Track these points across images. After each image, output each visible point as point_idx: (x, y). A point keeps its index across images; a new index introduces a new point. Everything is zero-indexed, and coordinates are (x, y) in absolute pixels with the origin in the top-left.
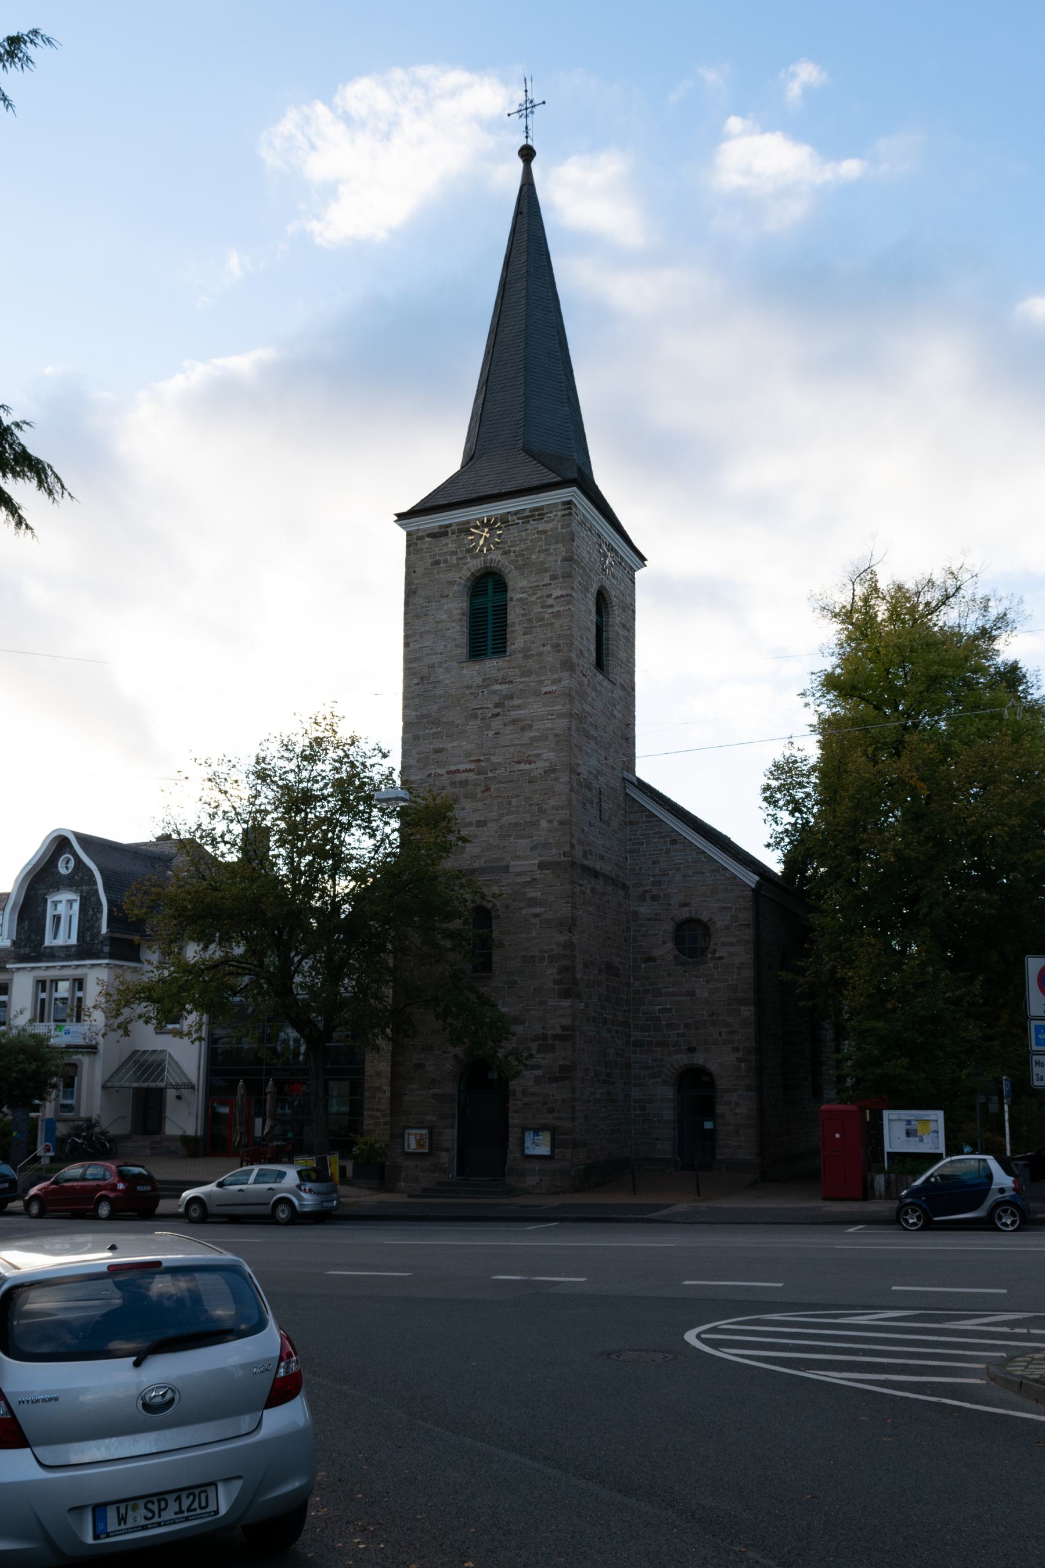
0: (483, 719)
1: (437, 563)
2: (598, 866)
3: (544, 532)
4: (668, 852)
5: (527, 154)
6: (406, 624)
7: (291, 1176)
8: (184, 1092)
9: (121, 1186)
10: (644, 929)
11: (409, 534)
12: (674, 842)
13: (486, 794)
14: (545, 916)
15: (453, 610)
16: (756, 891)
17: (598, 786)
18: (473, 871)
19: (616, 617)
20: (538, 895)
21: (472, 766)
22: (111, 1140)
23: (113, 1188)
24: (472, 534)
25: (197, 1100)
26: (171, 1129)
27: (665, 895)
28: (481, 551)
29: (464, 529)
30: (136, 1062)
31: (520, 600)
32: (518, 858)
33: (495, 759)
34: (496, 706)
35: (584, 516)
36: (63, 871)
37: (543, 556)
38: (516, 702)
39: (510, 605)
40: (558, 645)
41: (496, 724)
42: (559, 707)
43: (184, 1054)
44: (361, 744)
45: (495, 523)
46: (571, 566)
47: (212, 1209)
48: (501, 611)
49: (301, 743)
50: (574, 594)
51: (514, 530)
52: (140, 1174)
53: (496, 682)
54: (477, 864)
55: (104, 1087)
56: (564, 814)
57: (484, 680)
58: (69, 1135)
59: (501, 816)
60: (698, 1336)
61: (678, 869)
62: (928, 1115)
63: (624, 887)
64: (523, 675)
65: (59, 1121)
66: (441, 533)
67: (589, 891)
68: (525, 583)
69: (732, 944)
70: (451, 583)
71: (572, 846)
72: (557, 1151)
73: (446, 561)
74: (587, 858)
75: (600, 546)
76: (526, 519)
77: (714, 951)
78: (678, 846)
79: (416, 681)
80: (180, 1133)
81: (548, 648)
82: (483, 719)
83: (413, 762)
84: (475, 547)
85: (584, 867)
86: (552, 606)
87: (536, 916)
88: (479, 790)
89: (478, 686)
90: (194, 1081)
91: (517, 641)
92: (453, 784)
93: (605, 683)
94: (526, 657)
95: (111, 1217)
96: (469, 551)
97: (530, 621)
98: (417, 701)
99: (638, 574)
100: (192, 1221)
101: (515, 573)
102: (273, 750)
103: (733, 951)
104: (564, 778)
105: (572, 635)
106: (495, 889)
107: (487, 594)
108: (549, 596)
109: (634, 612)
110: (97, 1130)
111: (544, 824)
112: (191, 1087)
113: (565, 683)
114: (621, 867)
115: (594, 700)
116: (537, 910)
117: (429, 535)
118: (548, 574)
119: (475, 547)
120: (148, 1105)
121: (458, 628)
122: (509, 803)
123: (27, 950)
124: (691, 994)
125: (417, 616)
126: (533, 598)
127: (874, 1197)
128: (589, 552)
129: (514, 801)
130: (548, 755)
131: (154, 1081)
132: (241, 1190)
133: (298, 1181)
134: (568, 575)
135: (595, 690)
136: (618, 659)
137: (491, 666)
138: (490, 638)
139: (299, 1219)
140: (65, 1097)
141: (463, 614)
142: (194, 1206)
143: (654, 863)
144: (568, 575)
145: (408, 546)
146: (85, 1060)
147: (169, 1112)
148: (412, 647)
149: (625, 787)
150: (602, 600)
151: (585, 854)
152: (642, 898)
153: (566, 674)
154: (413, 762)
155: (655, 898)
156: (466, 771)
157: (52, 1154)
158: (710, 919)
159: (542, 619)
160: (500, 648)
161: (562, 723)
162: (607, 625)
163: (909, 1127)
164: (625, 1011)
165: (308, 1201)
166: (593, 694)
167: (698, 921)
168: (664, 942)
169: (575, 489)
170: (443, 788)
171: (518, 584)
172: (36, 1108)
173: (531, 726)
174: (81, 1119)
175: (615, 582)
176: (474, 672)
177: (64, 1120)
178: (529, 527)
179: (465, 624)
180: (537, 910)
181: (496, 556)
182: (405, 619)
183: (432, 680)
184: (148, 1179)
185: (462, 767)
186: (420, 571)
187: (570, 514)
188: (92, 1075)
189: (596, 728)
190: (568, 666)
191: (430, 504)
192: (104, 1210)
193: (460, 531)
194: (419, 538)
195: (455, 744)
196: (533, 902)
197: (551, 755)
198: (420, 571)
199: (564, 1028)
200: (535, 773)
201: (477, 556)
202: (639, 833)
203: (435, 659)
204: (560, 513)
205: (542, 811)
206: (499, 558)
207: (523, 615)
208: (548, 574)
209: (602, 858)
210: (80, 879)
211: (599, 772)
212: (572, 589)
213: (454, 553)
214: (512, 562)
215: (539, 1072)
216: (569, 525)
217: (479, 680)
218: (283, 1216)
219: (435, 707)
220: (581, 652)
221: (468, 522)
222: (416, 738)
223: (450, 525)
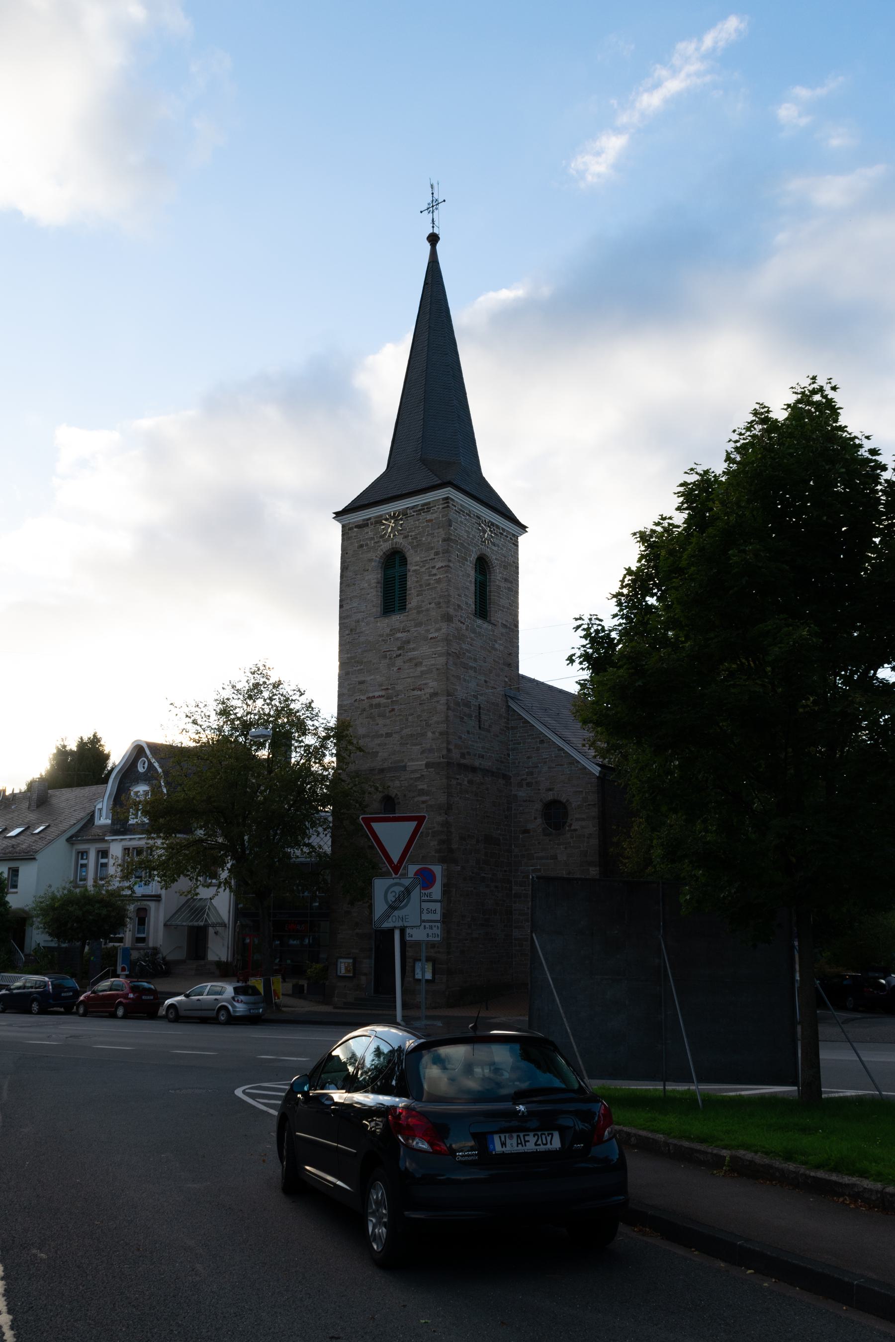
0: (390, 658)
1: (361, 546)
2: (477, 763)
3: (431, 521)
4: (538, 749)
5: (433, 239)
6: (341, 591)
7: (229, 990)
8: (219, 929)
9: (131, 996)
11: (343, 526)
12: (542, 742)
13: (393, 713)
14: (430, 803)
15: (372, 579)
16: (602, 779)
17: (477, 704)
18: (382, 771)
19: (497, 575)
20: (425, 787)
21: (383, 693)
22: (166, 963)
23: (125, 996)
24: (384, 524)
25: (228, 935)
26: (211, 957)
27: (536, 782)
28: (389, 536)
29: (378, 521)
30: (189, 906)
31: (415, 571)
32: (412, 760)
33: (399, 687)
34: (399, 649)
35: (461, 505)
36: (141, 769)
37: (429, 538)
38: (412, 646)
39: (409, 574)
40: (439, 603)
41: (399, 662)
42: (440, 649)
43: (221, 902)
44: (285, 686)
45: (399, 515)
46: (449, 545)
47: (182, 1013)
48: (404, 578)
49: (243, 686)
50: (451, 565)
51: (411, 521)
52: (150, 989)
53: (399, 631)
54: (386, 765)
55: (165, 925)
56: (443, 727)
57: (391, 630)
58: (138, 960)
59: (402, 729)
60: (244, 1092)
61: (545, 762)
63: (505, 777)
64: (415, 626)
65: (132, 949)
66: (362, 526)
67: (466, 783)
68: (418, 558)
69: (583, 819)
70: (370, 560)
71: (449, 750)
72: (436, 976)
73: (367, 545)
74: (465, 758)
75: (480, 525)
76: (419, 512)
77: (571, 825)
78: (545, 745)
79: (347, 632)
80: (217, 959)
81: (433, 605)
82: (390, 658)
83: (346, 691)
84: (385, 534)
85: (460, 765)
86: (435, 575)
87: (423, 802)
88: (388, 710)
89: (388, 635)
90: (226, 921)
91: (413, 601)
92: (371, 706)
93: (486, 625)
94: (419, 613)
95: (125, 1017)
96: (382, 537)
97: (421, 586)
98: (348, 647)
99: (522, 539)
100: (171, 1021)
101: (412, 551)
102: (228, 693)
103: (583, 824)
104: (443, 699)
105: (449, 595)
106: (397, 783)
107: (394, 562)
108: (434, 567)
109: (517, 568)
110: (160, 956)
111: (430, 734)
112: (224, 925)
113: (444, 631)
114: (502, 762)
116: (424, 798)
117: (357, 527)
118: (433, 551)
119: (385, 534)
120: (197, 938)
121: (375, 593)
122: (407, 720)
123: (119, 827)
124: (555, 857)
125: (348, 585)
126: (423, 569)
128: (467, 532)
129: (410, 718)
130: (433, 685)
131: (197, 921)
132: (198, 1000)
133: (233, 995)
134: (446, 551)
135: (474, 631)
136: (499, 605)
137: (396, 619)
138: (397, 599)
139: (234, 1020)
140: (138, 933)
141: (378, 583)
142: (171, 1011)
143: (528, 758)
144: (446, 551)
145: (343, 535)
146: (152, 905)
147: (210, 945)
148: (346, 607)
149: (507, 702)
150: (482, 565)
151: (463, 756)
152: (520, 785)
153: (444, 625)
154: (346, 691)
155: (529, 785)
156: (379, 697)
157: (127, 973)
158: (568, 801)
159: (429, 584)
160: (403, 608)
161: (442, 660)
162: (490, 582)
164: (505, 871)
165: (240, 1008)
166: (473, 635)
167: (559, 802)
168: (535, 818)
171: (414, 559)
172: (121, 940)
173: (421, 663)
174: (149, 948)
175: (495, 548)
176: (385, 625)
177: (138, 949)
179: (379, 589)
180: (424, 798)
181: (399, 539)
182: (341, 588)
183: (358, 631)
184: (149, 991)
185: (377, 694)
186: (350, 552)
187: (448, 506)
188: (158, 916)
189: (475, 660)
190: (448, 618)
191: (357, 504)
192: (120, 1012)
193: (376, 522)
194: (351, 529)
195: (372, 677)
196: (422, 792)
197: (434, 684)
198: (350, 552)
200: (424, 697)
201: (385, 541)
202: (518, 735)
203: (359, 616)
204: (441, 506)
205: (428, 725)
206: (401, 541)
207: (417, 582)
208: (433, 551)
209: (483, 757)
210: (149, 776)
212: (449, 561)
213: (372, 539)
214: (410, 543)
216: (447, 515)
217: (388, 631)
218: (223, 1018)
219: (360, 651)
220: (459, 606)
221: (381, 516)
222: (347, 674)
223: (370, 519)
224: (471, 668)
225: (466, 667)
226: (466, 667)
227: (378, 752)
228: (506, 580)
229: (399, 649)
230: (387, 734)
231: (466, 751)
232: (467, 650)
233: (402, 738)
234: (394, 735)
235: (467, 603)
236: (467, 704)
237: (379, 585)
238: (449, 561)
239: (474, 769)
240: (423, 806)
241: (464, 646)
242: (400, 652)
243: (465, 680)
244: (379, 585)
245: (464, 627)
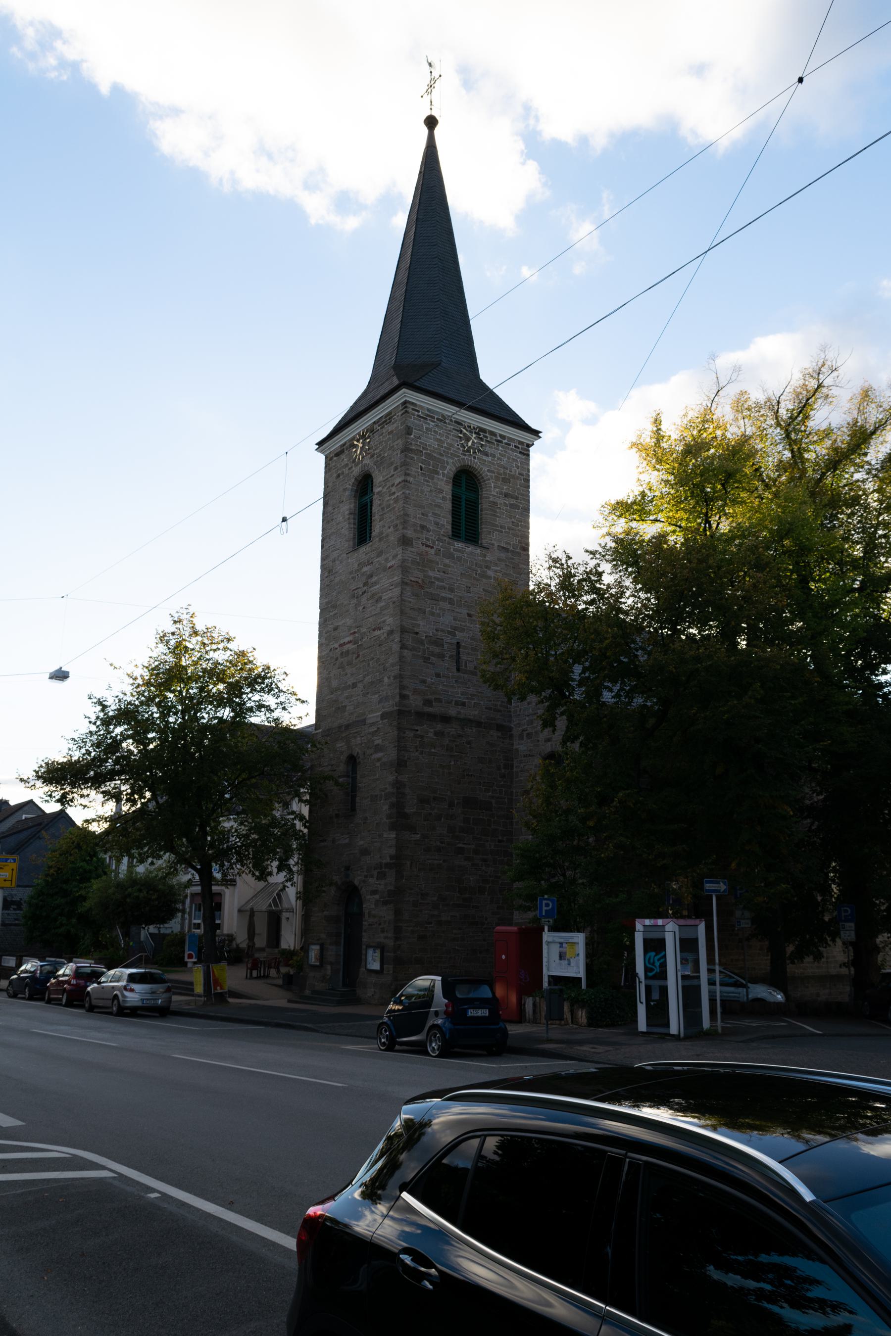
1: (338, 476)
2: (453, 712)
3: (392, 432)
5: (431, 122)
10: (522, 765)
11: (326, 458)
14: (384, 760)
17: (454, 641)
18: (348, 727)
35: (428, 410)
38: (374, 579)
39: (375, 497)
42: (396, 578)
51: (376, 436)
55: (239, 911)
59: (364, 677)
62: (572, 938)
64: (378, 556)
67: (431, 735)
70: (345, 490)
72: (385, 966)
74: (432, 706)
81: (392, 529)
83: (324, 641)
85: (420, 715)
87: (379, 760)
101: (377, 472)
108: (393, 485)
113: (399, 557)
115: (446, 565)
116: (380, 755)
122: (369, 665)
126: (385, 490)
127: (81, 1007)
135: (450, 556)
141: (350, 514)
150: (467, 481)
152: (521, 737)
156: (349, 642)
163: (561, 949)
164: (500, 841)
165: (135, 995)
166: (447, 561)
169: (404, 390)
170: (337, 660)
173: (381, 598)
174: (223, 935)
178: (384, 431)
185: (347, 640)
186: (330, 484)
187: (406, 412)
189: (452, 590)
196: (378, 748)
199: (391, 857)
201: (356, 465)
205: (385, 669)
209: (463, 704)
211: (455, 629)
215: (377, 897)
220: (423, 527)
222: (325, 621)
223: (345, 443)
224: (444, 599)
225: (435, 598)
226: (435, 598)
227: (345, 706)
228: (506, 495)
229: (365, 584)
230: (353, 684)
231: (433, 697)
232: (438, 579)
233: (364, 687)
234: (359, 685)
235: (437, 524)
236: (438, 643)
237: (352, 516)
238: (407, 474)
239: (446, 719)
240: (378, 764)
241: (431, 573)
242: (365, 588)
243: (433, 614)
244: (352, 516)
245: (433, 551)
